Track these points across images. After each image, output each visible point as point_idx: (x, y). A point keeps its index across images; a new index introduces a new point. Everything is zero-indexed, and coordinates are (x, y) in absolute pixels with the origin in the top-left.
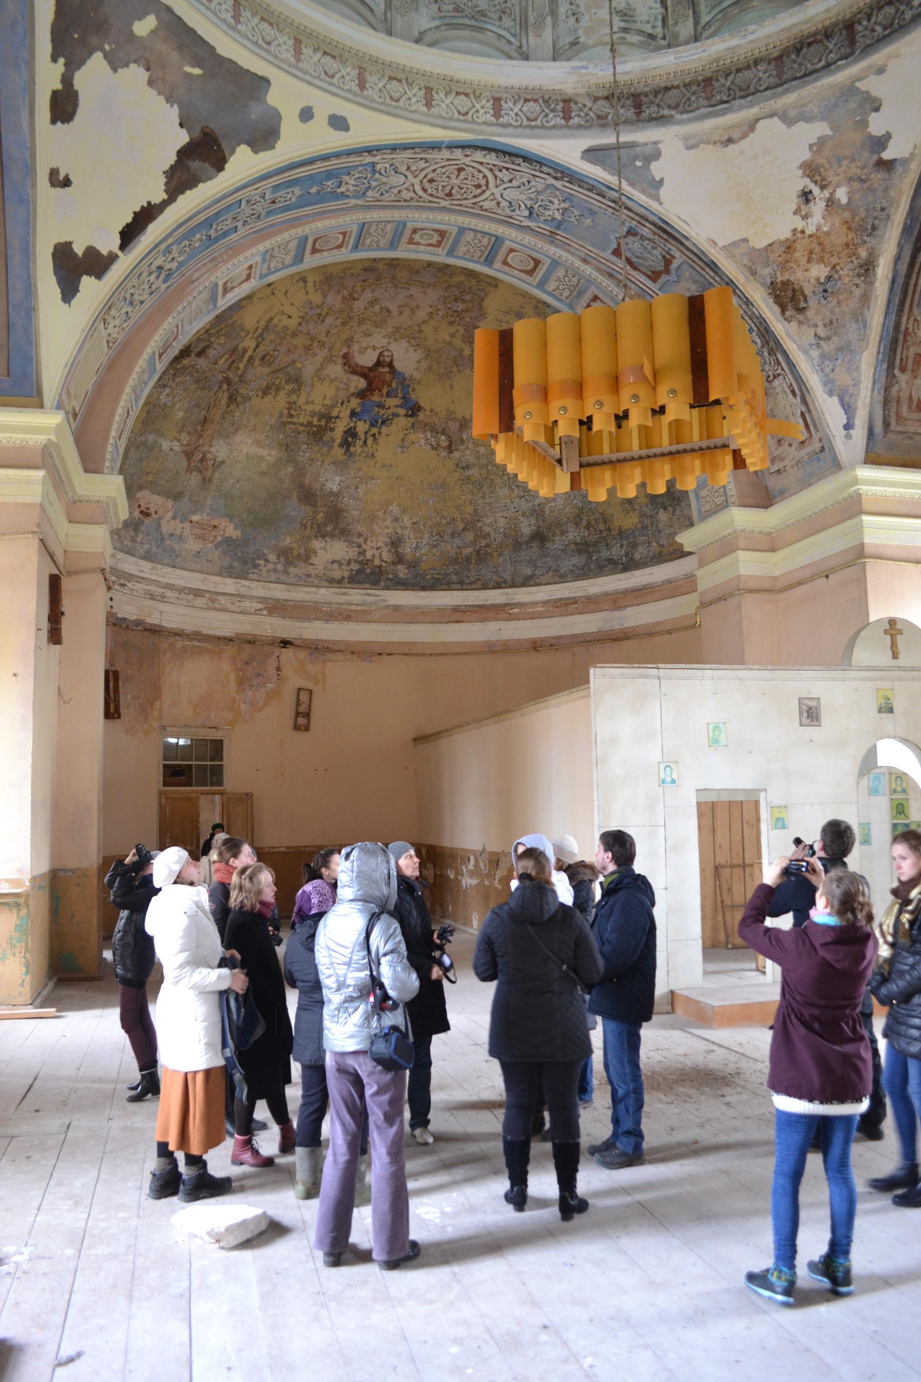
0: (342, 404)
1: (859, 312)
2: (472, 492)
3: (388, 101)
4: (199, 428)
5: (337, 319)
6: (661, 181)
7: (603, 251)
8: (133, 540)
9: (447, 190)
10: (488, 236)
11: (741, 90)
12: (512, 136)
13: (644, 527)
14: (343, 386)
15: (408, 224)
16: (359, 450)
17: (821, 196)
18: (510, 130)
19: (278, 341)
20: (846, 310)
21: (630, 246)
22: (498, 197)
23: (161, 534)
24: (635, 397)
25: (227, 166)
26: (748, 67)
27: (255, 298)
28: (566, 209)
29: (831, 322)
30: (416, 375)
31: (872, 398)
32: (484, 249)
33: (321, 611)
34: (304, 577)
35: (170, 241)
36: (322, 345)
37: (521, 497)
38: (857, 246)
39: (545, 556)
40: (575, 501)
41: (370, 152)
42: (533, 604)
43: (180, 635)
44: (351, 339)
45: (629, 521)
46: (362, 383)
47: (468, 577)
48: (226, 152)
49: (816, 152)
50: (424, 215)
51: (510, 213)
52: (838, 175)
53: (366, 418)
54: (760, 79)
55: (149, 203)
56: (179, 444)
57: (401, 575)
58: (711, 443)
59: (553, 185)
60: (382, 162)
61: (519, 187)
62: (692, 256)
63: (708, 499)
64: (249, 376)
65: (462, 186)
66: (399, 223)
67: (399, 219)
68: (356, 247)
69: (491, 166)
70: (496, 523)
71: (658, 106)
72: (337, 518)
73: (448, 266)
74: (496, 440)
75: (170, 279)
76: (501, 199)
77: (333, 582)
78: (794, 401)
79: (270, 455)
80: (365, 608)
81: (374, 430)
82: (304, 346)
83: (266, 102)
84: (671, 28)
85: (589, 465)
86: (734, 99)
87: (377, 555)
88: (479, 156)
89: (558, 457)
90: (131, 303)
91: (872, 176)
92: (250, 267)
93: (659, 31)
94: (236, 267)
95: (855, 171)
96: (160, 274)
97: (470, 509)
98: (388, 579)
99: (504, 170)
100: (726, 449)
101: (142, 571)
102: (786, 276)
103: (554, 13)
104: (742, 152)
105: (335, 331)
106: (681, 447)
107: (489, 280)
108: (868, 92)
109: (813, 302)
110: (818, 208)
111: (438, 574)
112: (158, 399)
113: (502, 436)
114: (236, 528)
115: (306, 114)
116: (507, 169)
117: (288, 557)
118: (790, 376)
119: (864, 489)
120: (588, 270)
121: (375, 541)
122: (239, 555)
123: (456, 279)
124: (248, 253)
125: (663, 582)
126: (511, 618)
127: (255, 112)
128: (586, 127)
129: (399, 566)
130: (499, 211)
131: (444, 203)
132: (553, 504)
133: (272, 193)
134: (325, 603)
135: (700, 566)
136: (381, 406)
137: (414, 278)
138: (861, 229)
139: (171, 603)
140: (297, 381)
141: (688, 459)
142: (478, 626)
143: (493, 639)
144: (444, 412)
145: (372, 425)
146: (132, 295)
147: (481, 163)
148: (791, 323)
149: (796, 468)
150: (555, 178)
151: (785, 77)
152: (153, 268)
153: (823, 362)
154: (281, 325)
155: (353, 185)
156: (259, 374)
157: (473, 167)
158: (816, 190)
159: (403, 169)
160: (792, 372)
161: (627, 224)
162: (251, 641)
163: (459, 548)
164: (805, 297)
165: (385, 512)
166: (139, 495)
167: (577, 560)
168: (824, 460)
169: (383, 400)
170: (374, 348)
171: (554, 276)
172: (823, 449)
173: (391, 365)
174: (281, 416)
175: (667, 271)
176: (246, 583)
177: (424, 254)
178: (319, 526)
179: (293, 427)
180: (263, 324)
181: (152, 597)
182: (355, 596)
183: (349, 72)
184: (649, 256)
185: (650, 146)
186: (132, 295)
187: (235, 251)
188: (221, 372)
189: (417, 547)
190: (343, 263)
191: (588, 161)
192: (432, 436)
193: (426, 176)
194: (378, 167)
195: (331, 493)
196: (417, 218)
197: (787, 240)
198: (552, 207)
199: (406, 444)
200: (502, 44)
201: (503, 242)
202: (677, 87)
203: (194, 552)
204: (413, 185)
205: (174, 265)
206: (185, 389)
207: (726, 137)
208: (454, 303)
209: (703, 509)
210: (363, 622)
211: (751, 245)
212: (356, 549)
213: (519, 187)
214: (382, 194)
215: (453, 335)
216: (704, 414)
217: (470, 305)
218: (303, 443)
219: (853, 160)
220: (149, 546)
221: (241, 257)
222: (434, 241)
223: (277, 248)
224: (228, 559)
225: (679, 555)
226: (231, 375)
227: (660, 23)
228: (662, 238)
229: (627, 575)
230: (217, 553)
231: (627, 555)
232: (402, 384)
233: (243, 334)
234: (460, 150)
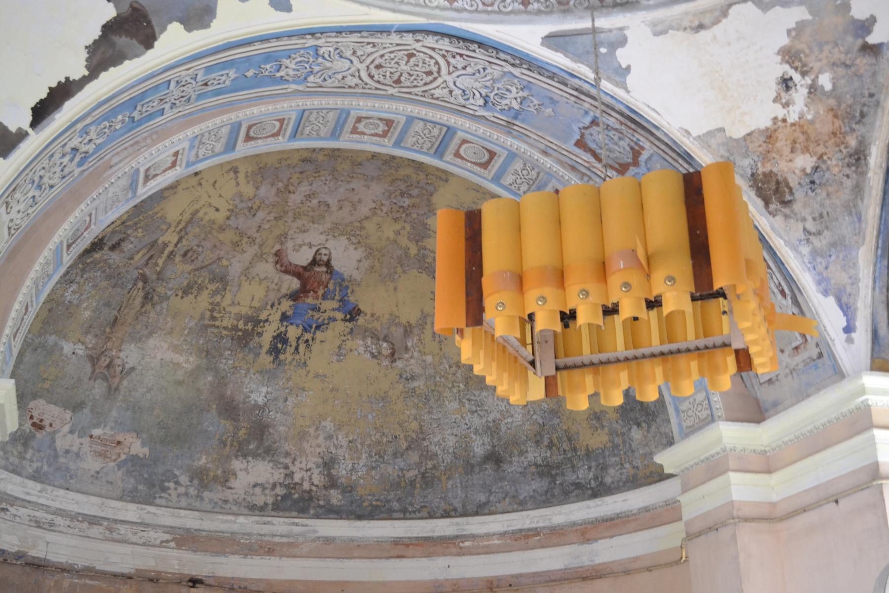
0: (272, 306)
1: (851, 204)
2: (417, 407)
4: (108, 330)
5: (270, 213)
6: (628, 69)
7: (565, 142)
8: (21, 457)
9: (396, 77)
10: (439, 127)
12: (466, 20)
13: (615, 446)
14: (273, 286)
15: (352, 113)
16: (290, 358)
17: (803, 82)
18: (465, 15)
19: (203, 236)
20: (838, 202)
21: (595, 136)
22: (451, 85)
23: (56, 450)
24: (627, 285)
25: (156, 44)
27: (180, 188)
28: (524, 98)
29: (821, 216)
30: (357, 275)
31: (873, 297)
33: (239, 543)
34: (220, 503)
35: (88, 120)
36: (253, 241)
37: (473, 412)
38: (844, 134)
39: (501, 479)
40: (535, 417)
41: (313, 34)
42: (488, 536)
43: (68, 571)
44: (285, 235)
45: (597, 440)
46: (295, 284)
47: (412, 504)
48: (157, 30)
49: (794, 38)
50: (370, 103)
52: (820, 60)
55: (67, 79)
56: (83, 347)
57: (334, 501)
58: (710, 341)
59: (510, 73)
60: (326, 45)
61: (474, 74)
62: (663, 147)
63: (690, 413)
64: (168, 274)
65: (411, 73)
66: (342, 110)
68: (294, 135)
70: (444, 441)
72: (262, 434)
73: (394, 157)
74: (462, 336)
75: (83, 163)
77: (254, 509)
78: (784, 302)
79: (187, 361)
80: (291, 540)
81: (308, 336)
82: (232, 241)
85: (566, 368)
87: (307, 478)
88: (430, 41)
89: (531, 358)
90: (39, 187)
91: (858, 61)
92: (176, 154)
94: (161, 152)
95: (838, 56)
96: (75, 156)
97: (414, 425)
98: (320, 506)
99: (458, 57)
100: (727, 349)
101: (28, 494)
102: (768, 168)
104: (715, 38)
105: (266, 226)
106: (674, 347)
107: (439, 174)
109: (799, 194)
110: (800, 95)
111: (377, 500)
112: (62, 295)
113: (468, 331)
114: (143, 444)
116: (461, 55)
117: (203, 479)
118: (778, 275)
119: (873, 400)
120: (548, 162)
121: (304, 462)
122: (146, 476)
123: (403, 172)
124: (175, 138)
125: (639, 509)
126: (462, 552)
128: (546, 13)
129: (332, 491)
130: (452, 100)
131: (391, 91)
132: (509, 420)
133: (204, 75)
134: (244, 534)
135: (684, 491)
136: (316, 309)
138: (849, 116)
139: (60, 532)
140: (222, 280)
141: (682, 360)
142: (424, 562)
143: (441, 578)
144: (387, 316)
145: (305, 330)
146: (41, 177)
147: (433, 49)
148: (777, 218)
149: (790, 377)
150: (513, 65)
152: (67, 149)
153: (814, 259)
154: (207, 218)
155: (294, 69)
156: (180, 271)
158: (797, 77)
159: (348, 53)
160: (780, 270)
161: (592, 114)
162: (154, 579)
163: (402, 470)
164: (791, 190)
165: (317, 429)
166: (32, 404)
167: (539, 485)
168: (823, 368)
169: (318, 302)
170: (310, 246)
171: (511, 169)
172: (820, 355)
173: (328, 264)
174: (202, 317)
175: (636, 163)
176: (152, 509)
177: (369, 145)
178: (240, 443)
179: (215, 331)
180: (187, 216)
181: (38, 525)
182: (281, 526)
184: (616, 148)
185: (615, 32)
186: (41, 177)
187: (161, 134)
188: (137, 268)
189: (353, 469)
190: (279, 152)
193: (373, 62)
194: (321, 51)
195: (256, 406)
197: (767, 129)
198: (509, 96)
199: (343, 351)
201: (455, 133)
203: (92, 472)
204: (359, 71)
205: (91, 147)
206: (95, 286)
207: (697, 23)
208: (400, 198)
210: (288, 557)
211: (728, 134)
212: (282, 470)
213: (474, 74)
214: (325, 80)
216: (699, 310)
217: (418, 200)
218: (226, 349)
219: (836, 45)
220: (39, 464)
221: (167, 142)
222: (380, 131)
223: (207, 134)
224: (132, 480)
225: (657, 478)
226: (147, 271)
228: (630, 128)
229: (598, 501)
230: (120, 473)
231: (596, 478)
232: (340, 285)
233: (164, 227)
234: (411, 35)
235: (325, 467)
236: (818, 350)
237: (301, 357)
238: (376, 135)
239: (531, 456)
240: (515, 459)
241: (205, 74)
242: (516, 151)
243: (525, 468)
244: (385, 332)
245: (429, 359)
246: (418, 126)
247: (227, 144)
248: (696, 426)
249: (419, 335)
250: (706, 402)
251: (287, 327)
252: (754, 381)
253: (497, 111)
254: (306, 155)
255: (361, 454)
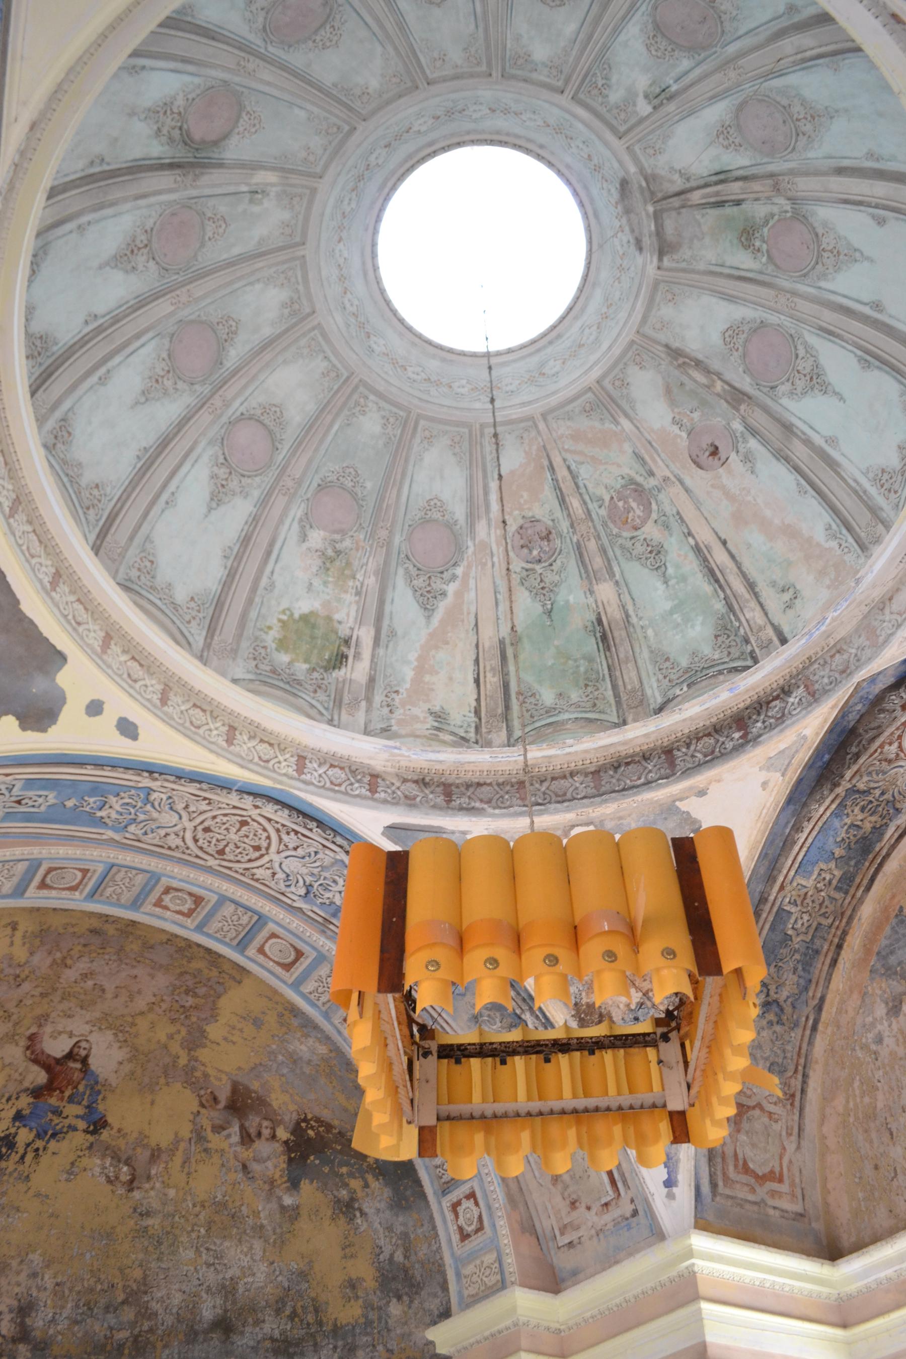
0: (8, 1100)
2: (146, 1251)
3: (188, 724)
5: (36, 987)
10: (250, 914)
11: (557, 795)
12: (313, 793)
13: (369, 1323)
18: (311, 788)
22: (276, 866)
26: (564, 777)
30: (113, 1081)
32: (240, 928)
37: (209, 1265)
40: (280, 1278)
41: (151, 772)
45: (348, 1313)
46: (40, 1077)
51: (283, 889)
53: (33, 1124)
54: (577, 788)
61: (303, 858)
63: (475, 1278)
65: (239, 844)
67: (155, 869)
69: (279, 826)
71: (469, 798)
76: (278, 870)
81: (39, 1144)
83: (54, 680)
84: (484, 735)
85: (449, 1118)
86: (550, 803)
88: (269, 810)
93: (472, 735)
97: (138, 1274)
99: (292, 834)
103: (369, 700)
105: (29, 1002)
108: (688, 813)
115: (95, 708)
119: (700, 1264)
123: (195, 965)
127: (38, 685)
130: (272, 884)
131: (212, 862)
132: (250, 1279)
136: (57, 1112)
137: (146, 955)
144: (135, 1135)
145: (38, 1136)
149: (595, 1239)
151: (603, 789)
155: (118, 812)
157: (259, 824)
163: (111, 1329)
165: (22, 1261)
169: (62, 1104)
170: (71, 1035)
171: (315, 976)
172: (635, 1213)
173: (84, 1061)
177: (169, 923)
183: (154, 685)
189: (53, 1320)
191: (389, 838)
192: (111, 1165)
196: (177, 874)
199: (75, 1170)
200: (313, 712)
202: (490, 784)
208: (183, 996)
209: (466, 1293)
213: (303, 858)
214: (146, 833)
215: (171, 1037)
222: (185, 909)
227: (473, 730)
232: (92, 1088)
234: (251, 798)
235: (19, 1312)
236: (633, 1207)
237: (24, 1168)
238: (179, 912)
239: (267, 1328)
240: (248, 1329)
241: (24, 788)
242: (327, 954)
243: (259, 1342)
244: (130, 1152)
245: (172, 1193)
246: (228, 910)
247: (18, 886)
248: (481, 1294)
249: (167, 1162)
250: (497, 1265)
251: (18, 1128)
252: (551, 1244)
253: (316, 905)
254: (96, 923)
255: (67, 1302)
